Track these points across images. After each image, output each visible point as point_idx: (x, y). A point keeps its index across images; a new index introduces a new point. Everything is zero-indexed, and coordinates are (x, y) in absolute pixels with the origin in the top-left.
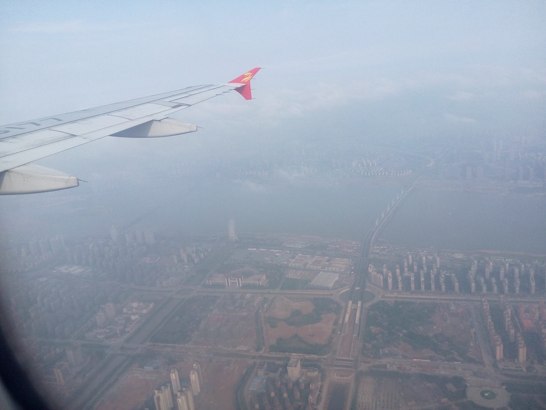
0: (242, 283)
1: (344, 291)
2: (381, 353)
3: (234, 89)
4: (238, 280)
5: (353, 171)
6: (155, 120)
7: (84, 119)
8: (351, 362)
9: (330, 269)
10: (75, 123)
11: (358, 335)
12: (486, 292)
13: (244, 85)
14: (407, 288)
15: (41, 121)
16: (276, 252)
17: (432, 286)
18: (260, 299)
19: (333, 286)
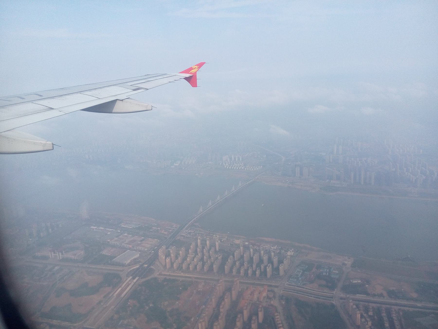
3: (184, 78)
4: (59, 254)
11: (114, 308)
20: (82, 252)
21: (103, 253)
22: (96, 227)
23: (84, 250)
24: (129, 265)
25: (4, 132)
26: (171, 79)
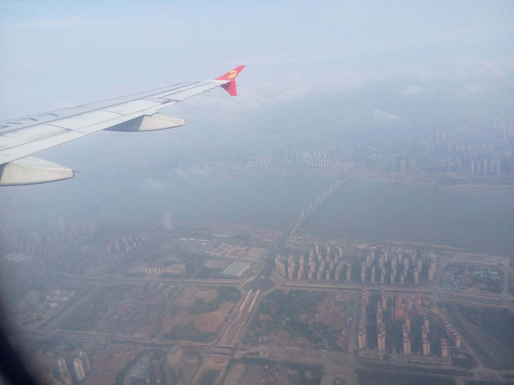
0: (133, 271)
1: (249, 280)
2: (260, 341)
3: (220, 86)
4: (157, 269)
5: (302, 162)
6: (146, 115)
7: (79, 114)
8: (229, 350)
9: (245, 259)
10: (71, 118)
11: (246, 324)
12: (375, 282)
13: (229, 81)
14: (305, 277)
15: (6, 123)
16: (193, 240)
17: (335, 276)
18: (171, 288)
19: (242, 275)
20: (183, 266)
21: (206, 266)
22: (186, 239)
23: (184, 264)
24: (242, 277)
25: (16, 160)
26: (206, 88)
